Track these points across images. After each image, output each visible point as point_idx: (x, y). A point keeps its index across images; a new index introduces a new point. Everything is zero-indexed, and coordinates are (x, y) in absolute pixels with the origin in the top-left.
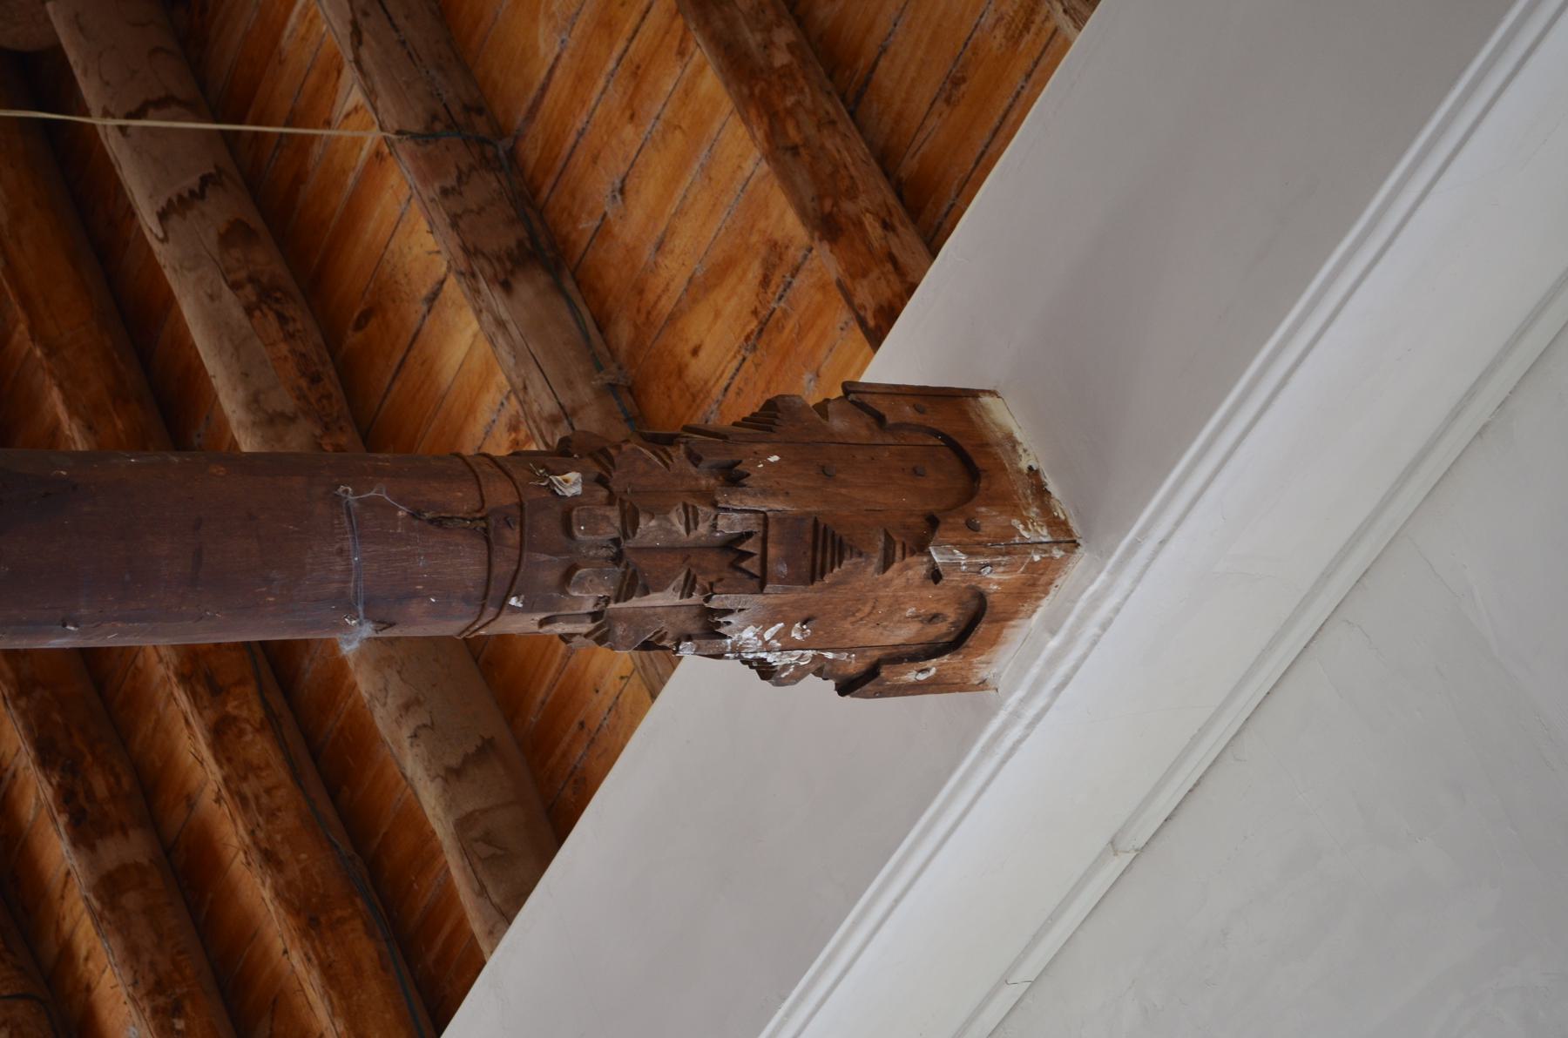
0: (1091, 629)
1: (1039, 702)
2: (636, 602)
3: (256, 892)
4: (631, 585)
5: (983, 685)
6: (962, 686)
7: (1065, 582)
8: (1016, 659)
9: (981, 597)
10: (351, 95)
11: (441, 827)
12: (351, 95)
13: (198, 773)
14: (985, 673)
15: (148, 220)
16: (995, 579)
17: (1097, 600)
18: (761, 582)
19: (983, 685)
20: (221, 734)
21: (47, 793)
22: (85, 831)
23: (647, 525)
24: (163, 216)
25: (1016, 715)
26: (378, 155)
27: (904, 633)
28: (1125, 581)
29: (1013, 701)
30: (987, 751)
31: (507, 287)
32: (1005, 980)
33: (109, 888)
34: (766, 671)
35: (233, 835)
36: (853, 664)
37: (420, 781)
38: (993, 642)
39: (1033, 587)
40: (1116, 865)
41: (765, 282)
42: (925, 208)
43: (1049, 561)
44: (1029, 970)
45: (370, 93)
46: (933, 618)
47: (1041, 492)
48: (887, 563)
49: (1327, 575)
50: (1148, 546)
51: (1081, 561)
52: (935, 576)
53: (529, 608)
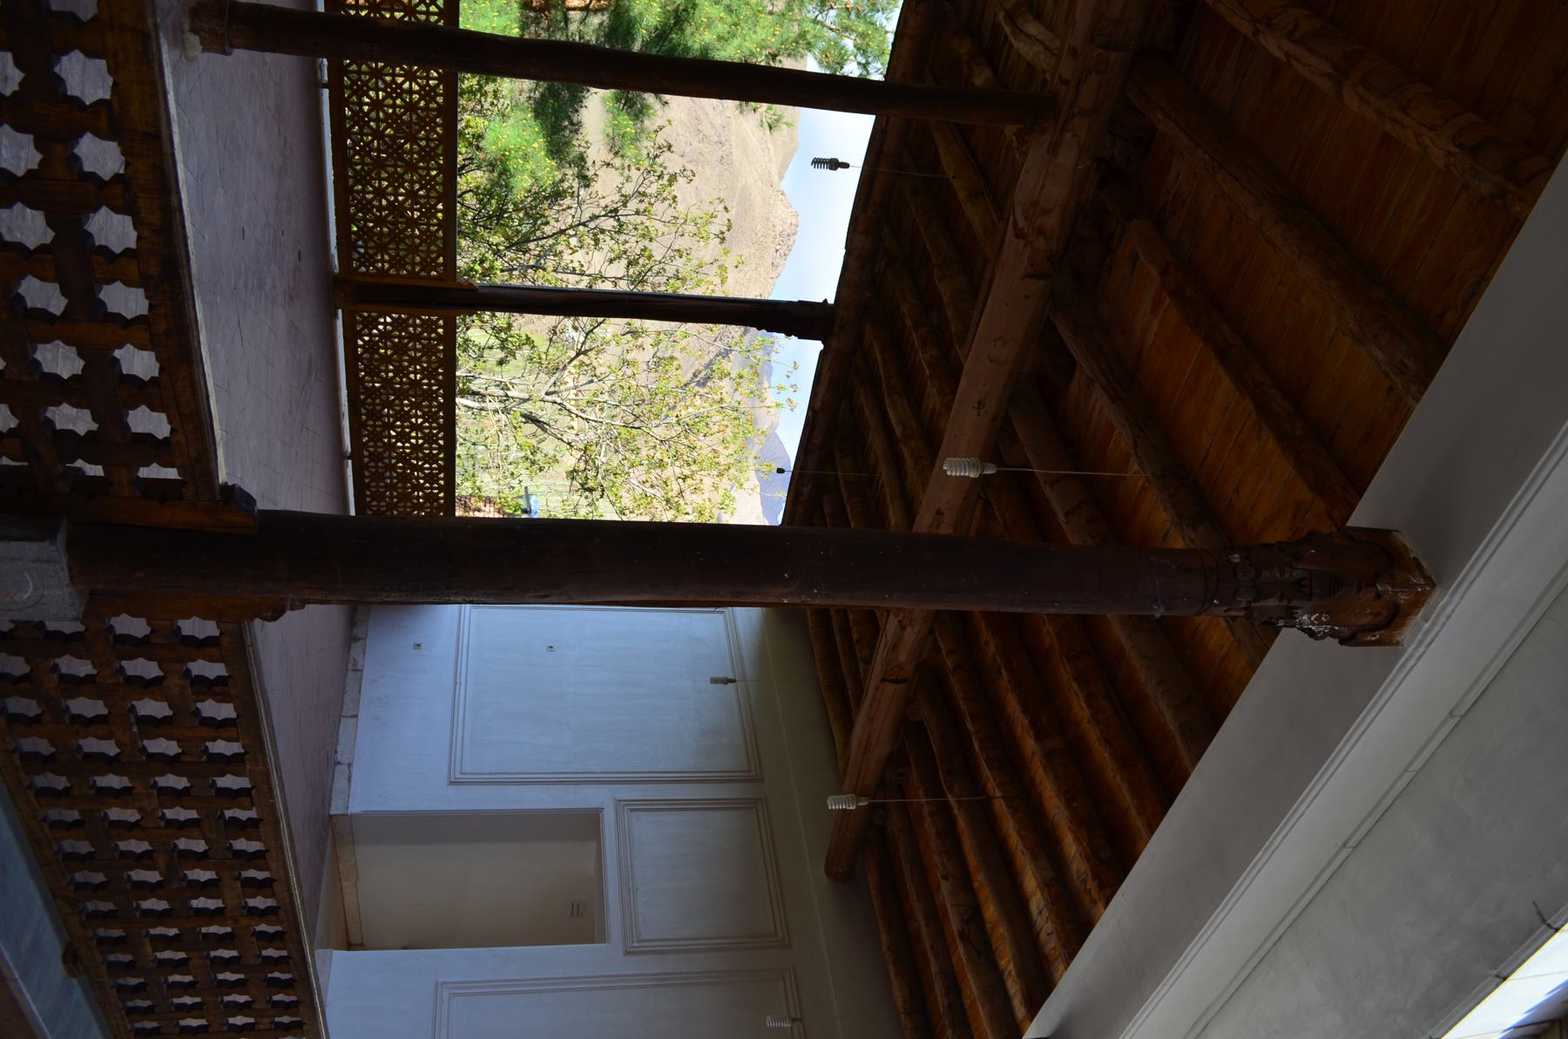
0: (1443, 619)
1: (1421, 650)
2: (1262, 603)
3: (1102, 755)
4: (1261, 595)
5: (1398, 643)
6: (1390, 643)
7: (1431, 601)
8: (1412, 634)
9: (1397, 606)
10: (1134, 467)
11: (1172, 726)
12: (1134, 467)
13: (1042, 904)
14: (1399, 638)
15: (1061, 517)
16: (1403, 598)
17: (1446, 606)
18: (1310, 596)
19: (1398, 643)
20: (1090, 699)
21: (1026, 722)
22: (1039, 736)
23: (1266, 574)
24: (1066, 515)
25: (1412, 655)
26: (1143, 489)
27: (1365, 620)
28: (1456, 599)
29: (1410, 650)
30: (1400, 670)
31: (1194, 528)
32: (1406, 770)
33: (1048, 756)
34: (1311, 634)
35: (1093, 735)
36: (1346, 631)
37: (1165, 712)
38: (1402, 625)
39: (1418, 602)
40: (1453, 721)
41: (1295, 517)
42: (1359, 484)
43: (1424, 591)
44: (1417, 766)
45: (1141, 464)
46: (1378, 614)
47: (1420, 566)
48: (1359, 591)
49: (1540, 599)
50: (1466, 584)
51: (1437, 592)
52: (1379, 596)
53: (1221, 604)
